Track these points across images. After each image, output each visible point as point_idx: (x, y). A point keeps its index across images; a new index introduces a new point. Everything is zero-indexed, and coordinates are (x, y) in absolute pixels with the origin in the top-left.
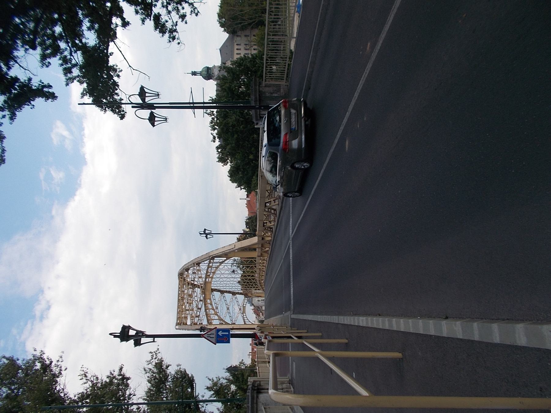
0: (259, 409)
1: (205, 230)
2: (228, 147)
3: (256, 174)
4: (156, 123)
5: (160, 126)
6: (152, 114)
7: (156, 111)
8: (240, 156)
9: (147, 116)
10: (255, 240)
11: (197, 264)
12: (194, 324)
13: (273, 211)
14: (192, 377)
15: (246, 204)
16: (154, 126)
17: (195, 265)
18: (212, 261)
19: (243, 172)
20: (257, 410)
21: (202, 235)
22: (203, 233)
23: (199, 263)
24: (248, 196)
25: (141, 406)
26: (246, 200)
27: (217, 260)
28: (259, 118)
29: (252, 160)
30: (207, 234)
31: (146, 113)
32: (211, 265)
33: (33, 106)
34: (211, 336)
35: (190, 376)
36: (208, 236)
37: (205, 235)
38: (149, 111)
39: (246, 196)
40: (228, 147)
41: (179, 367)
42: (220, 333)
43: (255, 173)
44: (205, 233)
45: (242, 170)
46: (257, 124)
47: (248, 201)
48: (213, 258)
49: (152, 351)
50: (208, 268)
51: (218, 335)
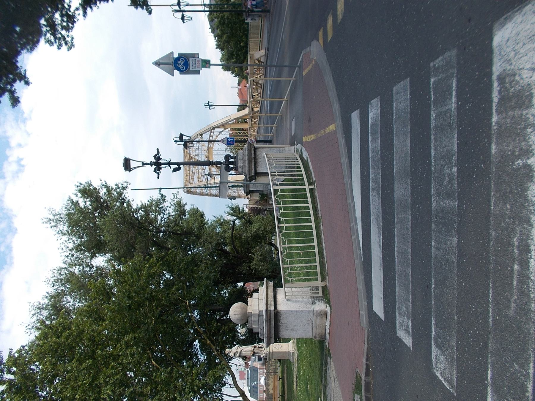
0: (250, 186)
1: (209, 102)
2: (225, 36)
3: (247, 59)
4: (185, 21)
5: (188, 23)
6: (183, 15)
7: (186, 14)
8: (233, 43)
9: (180, 16)
10: (246, 111)
11: (200, 135)
12: (200, 181)
13: (259, 85)
14: (203, 212)
15: (237, 93)
16: (184, 23)
17: (199, 136)
18: (213, 131)
19: (236, 58)
20: (249, 187)
21: (206, 107)
22: (207, 105)
23: (202, 135)
24: (239, 85)
25: (188, 177)
26: (237, 89)
27: (216, 130)
28: (248, 15)
29: (243, 47)
30: (210, 106)
31: (180, 14)
32: (212, 134)
33: (98, 7)
34: (225, 141)
35: (201, 211)
36: (211, 108)
37: (209, 107)
38: (181, 13)
39: (237, 85)
40: (225, 36)
41: (193, 206)
42: (229, 140)
43: (246, 58)
44: (209, 105)
45: (235, 55)
46: (247, 20)
47: (240, 90)
48: (214, 129)
49: (175, 193)
50: (210, 136)
51: (228, 141)
